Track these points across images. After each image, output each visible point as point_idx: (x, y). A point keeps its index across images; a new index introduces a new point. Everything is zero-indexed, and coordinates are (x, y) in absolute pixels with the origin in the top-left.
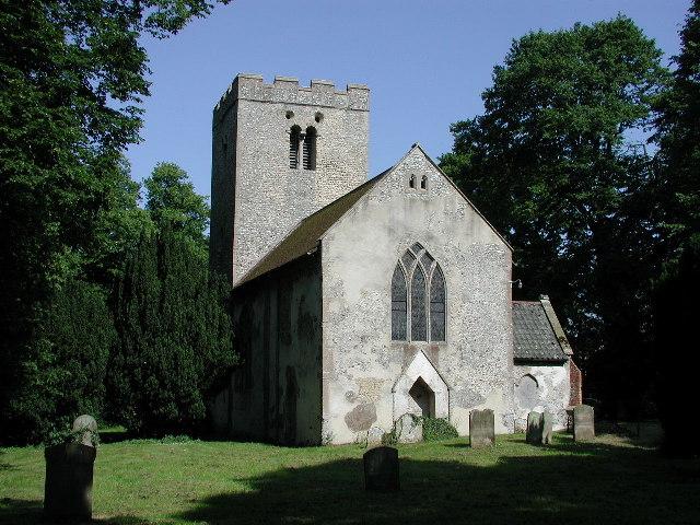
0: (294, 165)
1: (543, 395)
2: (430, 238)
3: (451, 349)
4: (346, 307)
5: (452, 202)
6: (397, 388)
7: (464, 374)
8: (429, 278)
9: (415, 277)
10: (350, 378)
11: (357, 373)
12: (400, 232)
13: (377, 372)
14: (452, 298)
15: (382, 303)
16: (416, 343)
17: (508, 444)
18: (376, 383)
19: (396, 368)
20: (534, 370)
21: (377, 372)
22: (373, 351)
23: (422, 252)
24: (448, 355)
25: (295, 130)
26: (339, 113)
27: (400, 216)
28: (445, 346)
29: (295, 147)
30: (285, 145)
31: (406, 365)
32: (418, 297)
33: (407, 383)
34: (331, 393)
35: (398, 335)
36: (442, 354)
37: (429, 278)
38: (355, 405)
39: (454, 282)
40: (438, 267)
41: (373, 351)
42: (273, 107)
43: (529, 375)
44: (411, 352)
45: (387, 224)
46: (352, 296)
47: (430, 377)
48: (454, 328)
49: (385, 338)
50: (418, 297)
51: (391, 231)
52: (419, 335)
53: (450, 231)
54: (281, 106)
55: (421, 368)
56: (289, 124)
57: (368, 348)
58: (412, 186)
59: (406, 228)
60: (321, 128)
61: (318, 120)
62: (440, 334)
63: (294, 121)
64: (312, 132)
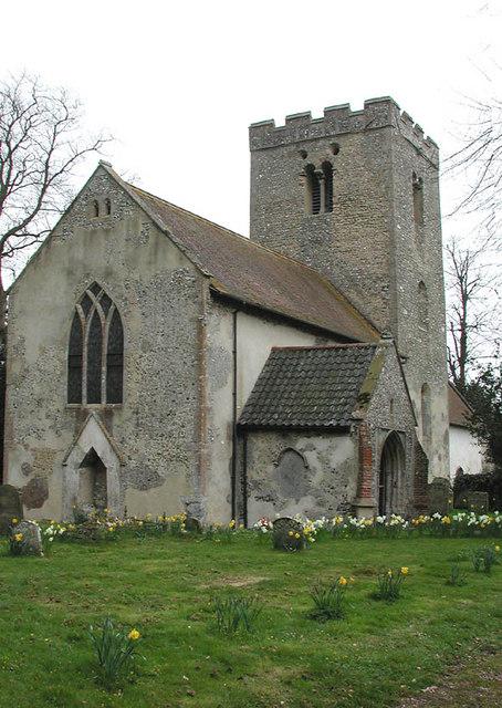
1: (315, 480)
2: (109, 274)
3: (127, 413)
4: (26, 366)
5: (136, 225)
6: (68, 462)
7: (140, 444)
8: (106, 324)
9: (92, 324)
10: (26, 447)
11: (33, 442)
12: (79, 274)
13: (50, 441)
14: (131, 349)
15: (58, 360)
16: (89, 406)
17: (448, 564)
18: (50, 453)
19: (68, 436)
20: (301, 443)
21: (50, 441)
22: (48, 416)
24: (124, 418)
25: (310, 168)
26: (356, 137)
27: (79, 253)
28: (120, 409)
30: (304, 191)
31: (78, 432)
33: (77, 457)
34: (10, 465)
35: (74, 396)
36: (116, 420)
37: (106, 324)
38: (29, 479)
39: (133, 326)
40: (116, 310)
41: (48, 416)
42: (284, 151)
43: (290, 450)
44: (82, 416)
45: (67, 266)
46: (32, 355)
47: (103, 450)
48: (132, 384)
49: (59, 400)
51: (70, 273)
52: (95, 398)
53: (130, 263)
54: (293, 148)
55: (94, 437)
56: (299, 165)
57: (43, 414)
59: (85, 266)
60: (338, 164)
62: (116, 396)
63: (308, 161)
64: (328, 167)
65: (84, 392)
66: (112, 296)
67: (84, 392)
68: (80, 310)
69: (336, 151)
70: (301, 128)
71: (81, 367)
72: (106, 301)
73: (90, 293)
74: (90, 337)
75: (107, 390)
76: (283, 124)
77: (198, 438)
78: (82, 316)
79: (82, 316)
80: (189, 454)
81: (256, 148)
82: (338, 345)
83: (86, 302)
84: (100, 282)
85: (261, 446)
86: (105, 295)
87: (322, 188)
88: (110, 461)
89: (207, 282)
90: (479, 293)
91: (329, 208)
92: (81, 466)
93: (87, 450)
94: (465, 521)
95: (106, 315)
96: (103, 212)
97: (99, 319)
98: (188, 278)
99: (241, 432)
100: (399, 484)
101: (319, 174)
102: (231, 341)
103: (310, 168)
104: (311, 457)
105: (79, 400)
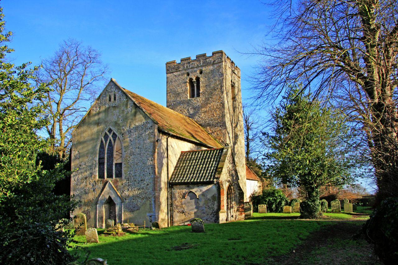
25: (191, 80)
35: (101, 176)
58: (110, 100)
61: (201, 73)
63: (190, 77)
64: (198, 79)
65: (114, 172)
67: (114, 172)
68: (103, 140)
71: (104, 163)
75: (116, 172)
76: (195, 58)
77: (154, 190)
78: (104, 142)
79: (104, 142)
80: (150, 196)
81: (168, 71)
83: (106, 137)
84: (112, 128)
85: (178, 192)
86: (114, 133)
87: (195, 87)
88: (117, 201)
89: (156, 126)
90: (254, 126)
94: (46, 239)
96: (112, 100)
97: (112, 143)
98: (149, 125)
99: (171, 185)
101: (194, 82)
102: (186, 143)
103: (191, 80)
105: (104, 178)
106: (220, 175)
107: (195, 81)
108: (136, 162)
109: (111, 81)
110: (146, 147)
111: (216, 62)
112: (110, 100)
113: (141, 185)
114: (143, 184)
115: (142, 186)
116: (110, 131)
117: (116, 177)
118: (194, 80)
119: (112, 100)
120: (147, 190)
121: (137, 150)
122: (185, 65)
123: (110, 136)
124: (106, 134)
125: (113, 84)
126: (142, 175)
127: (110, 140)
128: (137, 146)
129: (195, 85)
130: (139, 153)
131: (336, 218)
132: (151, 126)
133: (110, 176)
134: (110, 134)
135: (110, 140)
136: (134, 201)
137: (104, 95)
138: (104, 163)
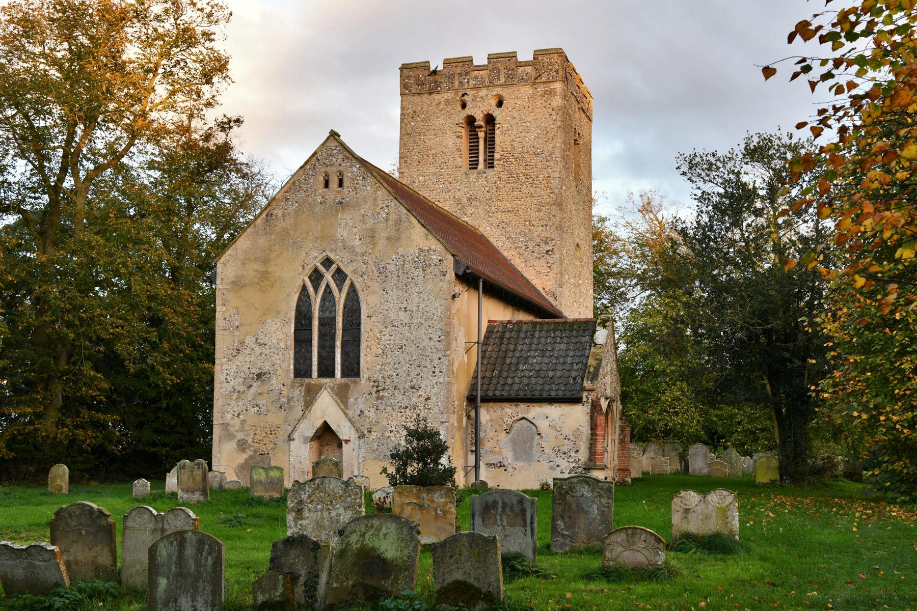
0: (474, 165)
6: (296, 435)
23: (334, 267)
24: (360, 398)
25: (471, 120)
29: (474, 138)
31: (308, 404)
32: (327, 324)
33: (309, 428)
35: (302, 371)
37: (341, 300)
38: (250, 453)
40: (352, 285)
44: (311, 394)
48: (367, 360)
50: (327, 324)
58: (327, 185)
61: (500, 104)
62: (352, 369)
63: (469, 111)
64: (490, 120)
66: (347, 270)
69: (500, 104)
70: (460, 75)
72: (340, 276)
73: (322, 269)
74: (320, 311)
79: (311, 289)
82: (538, 320)
83: (316, 277)
88: (344, 430)
91: (490, 164)
92: (312, 439)
93: (319, 424)
95: (340, 291)
96: (334, 184)
97: (331, 292)
100: (609, 449)
101: (481, 127)
103: (471, 120)
104: (543, 425)
105: (308, 374)
106: (622, 392)
107: (482, 123)
108: (397, 341)
109: (334, 135)
110: (427, 309)
111: (544, 79)
112: (327, 185)
113: (410, 399)
114: (416, 395)
115: (414, 400)
116: (328, 263)
117: (344, 375)
118: (480, 122)
119: (334, 184)
120: (426, 411)
121: (402, 314)
122: (456, 77)
123: (328, 277)
124: (316, 270)
125: (336, 144)
126: (413, 374)
127: (328, 286)
128: (400, 305)
129: (481, 135)
130: (406, 321)
131: (315, 309)
132: (440, 261)
133: (327, 371)
134: (327, 270)
135: (328, 286)
136: (392, 434)
137: (311, 172)
138: (310, 341)
